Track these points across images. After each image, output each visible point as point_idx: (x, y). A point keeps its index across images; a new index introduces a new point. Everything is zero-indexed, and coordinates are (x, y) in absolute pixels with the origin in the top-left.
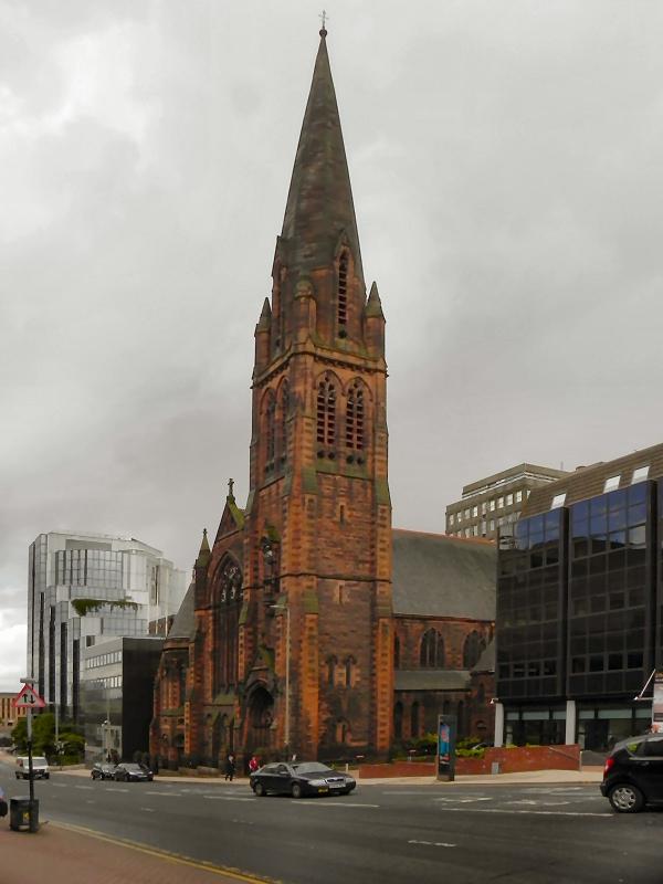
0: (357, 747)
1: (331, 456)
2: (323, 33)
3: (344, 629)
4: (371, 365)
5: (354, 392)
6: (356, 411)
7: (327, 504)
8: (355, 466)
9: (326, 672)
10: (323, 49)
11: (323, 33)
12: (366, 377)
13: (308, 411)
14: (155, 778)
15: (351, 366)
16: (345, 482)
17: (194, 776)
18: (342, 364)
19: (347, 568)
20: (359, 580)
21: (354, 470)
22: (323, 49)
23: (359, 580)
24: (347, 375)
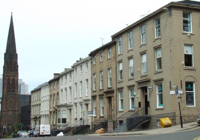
0: (196, 104)
1: (10, 91)
2: (12, 13)
3: (11, 119)
4: (15, 75)
5: (13, 80)
6: (14, 83)
7: (9, 99)
8: (13, 92)
9: (8, 127)
10: (12, 15)
11: (12, 13)
12: (15, 77)
13: (6, 85)
14: (157, 86)
15: (13, 76)
16: (11, 95)
17: (122, 132)
18: (11, 76)
19: (11, 109)
20: (13, 111)
21: (13, 93)
22: (12, 15)
23: (13, 111)
24: (12, 78)
